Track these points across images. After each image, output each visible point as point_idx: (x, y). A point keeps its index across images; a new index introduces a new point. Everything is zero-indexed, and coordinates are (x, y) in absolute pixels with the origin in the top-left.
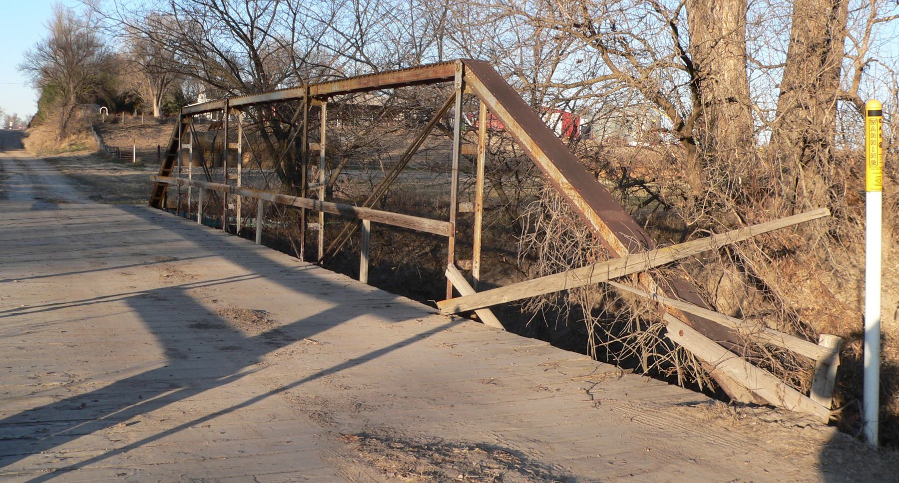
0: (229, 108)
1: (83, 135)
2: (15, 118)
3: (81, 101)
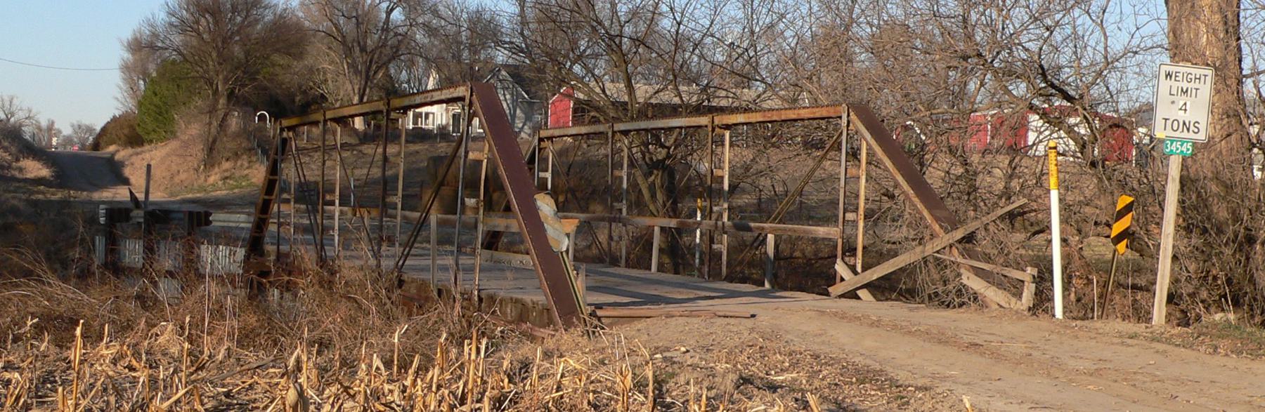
0: (614, 133)
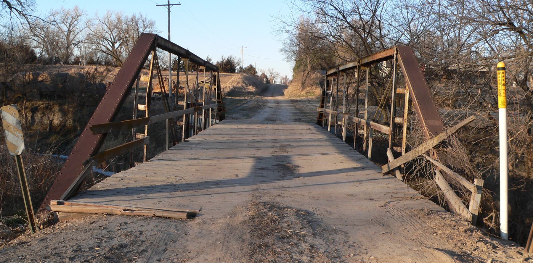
1: (314, 87)
2: (286, 78)
3: (314, 69)
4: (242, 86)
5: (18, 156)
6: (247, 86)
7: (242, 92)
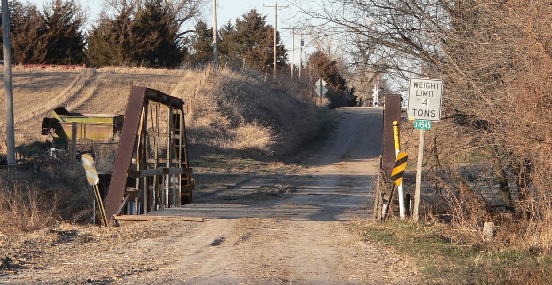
4: (214, 124)
5: (95, 186)
6: (235, 125)
7: (218, 150)
